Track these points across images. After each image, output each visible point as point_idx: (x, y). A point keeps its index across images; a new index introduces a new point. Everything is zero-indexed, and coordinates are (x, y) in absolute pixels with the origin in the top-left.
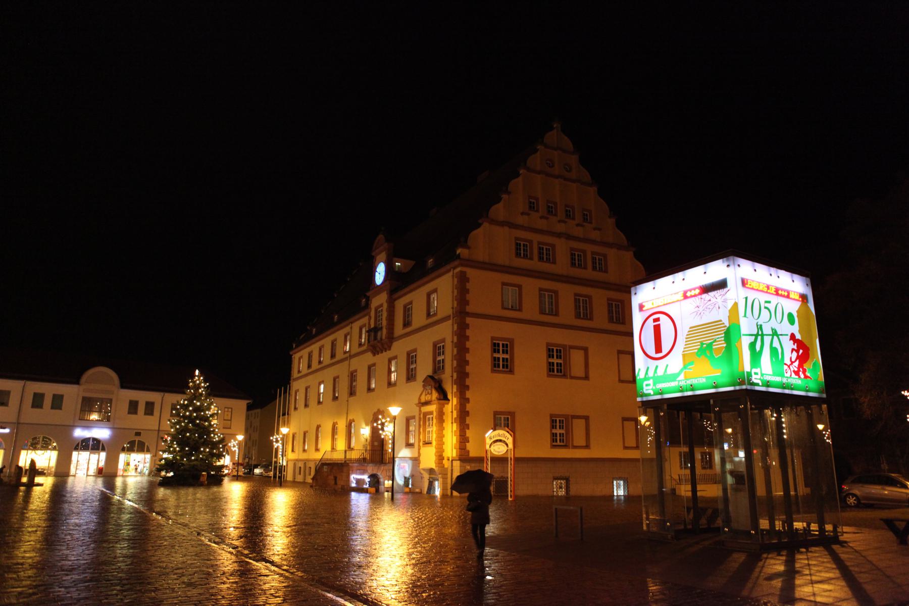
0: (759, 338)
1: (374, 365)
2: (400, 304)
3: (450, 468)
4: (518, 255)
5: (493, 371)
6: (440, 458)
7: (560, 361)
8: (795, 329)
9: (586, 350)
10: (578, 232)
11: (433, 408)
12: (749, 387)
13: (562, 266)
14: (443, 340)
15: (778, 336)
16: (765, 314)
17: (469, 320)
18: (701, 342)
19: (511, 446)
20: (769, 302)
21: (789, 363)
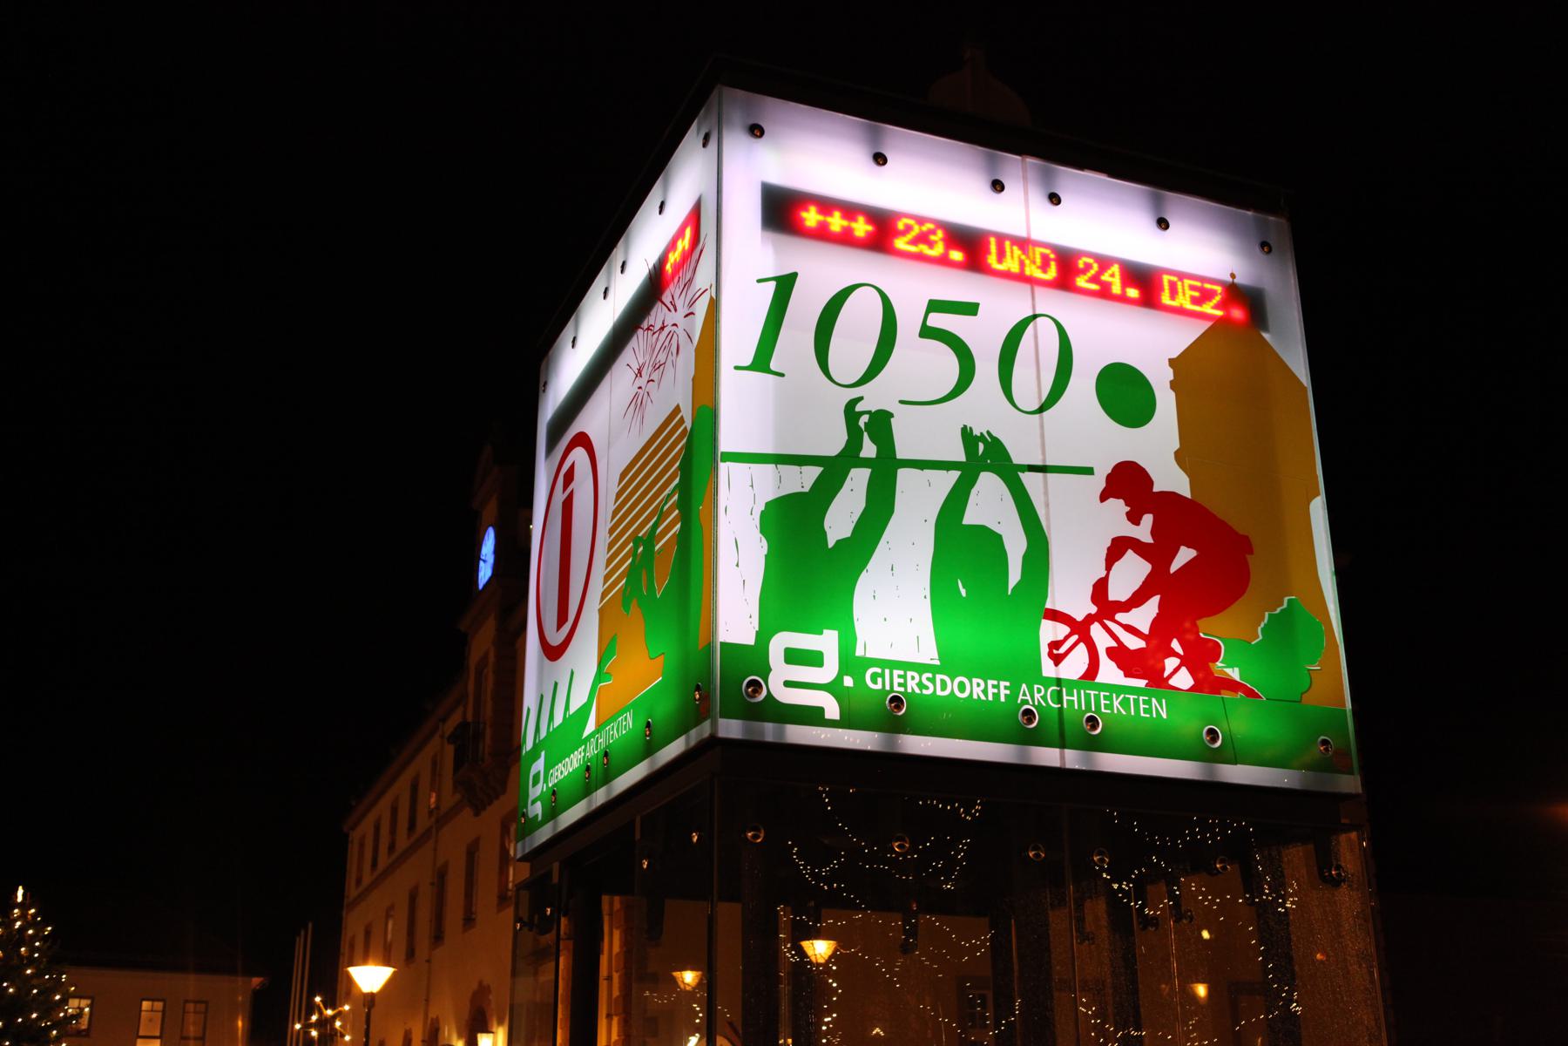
0: (858, 479)
8: (1157, 448)
12: (731, 728)
15: (1010, 473)
16: (921, 367)
20: (970, 309)
21: (1081, 607)
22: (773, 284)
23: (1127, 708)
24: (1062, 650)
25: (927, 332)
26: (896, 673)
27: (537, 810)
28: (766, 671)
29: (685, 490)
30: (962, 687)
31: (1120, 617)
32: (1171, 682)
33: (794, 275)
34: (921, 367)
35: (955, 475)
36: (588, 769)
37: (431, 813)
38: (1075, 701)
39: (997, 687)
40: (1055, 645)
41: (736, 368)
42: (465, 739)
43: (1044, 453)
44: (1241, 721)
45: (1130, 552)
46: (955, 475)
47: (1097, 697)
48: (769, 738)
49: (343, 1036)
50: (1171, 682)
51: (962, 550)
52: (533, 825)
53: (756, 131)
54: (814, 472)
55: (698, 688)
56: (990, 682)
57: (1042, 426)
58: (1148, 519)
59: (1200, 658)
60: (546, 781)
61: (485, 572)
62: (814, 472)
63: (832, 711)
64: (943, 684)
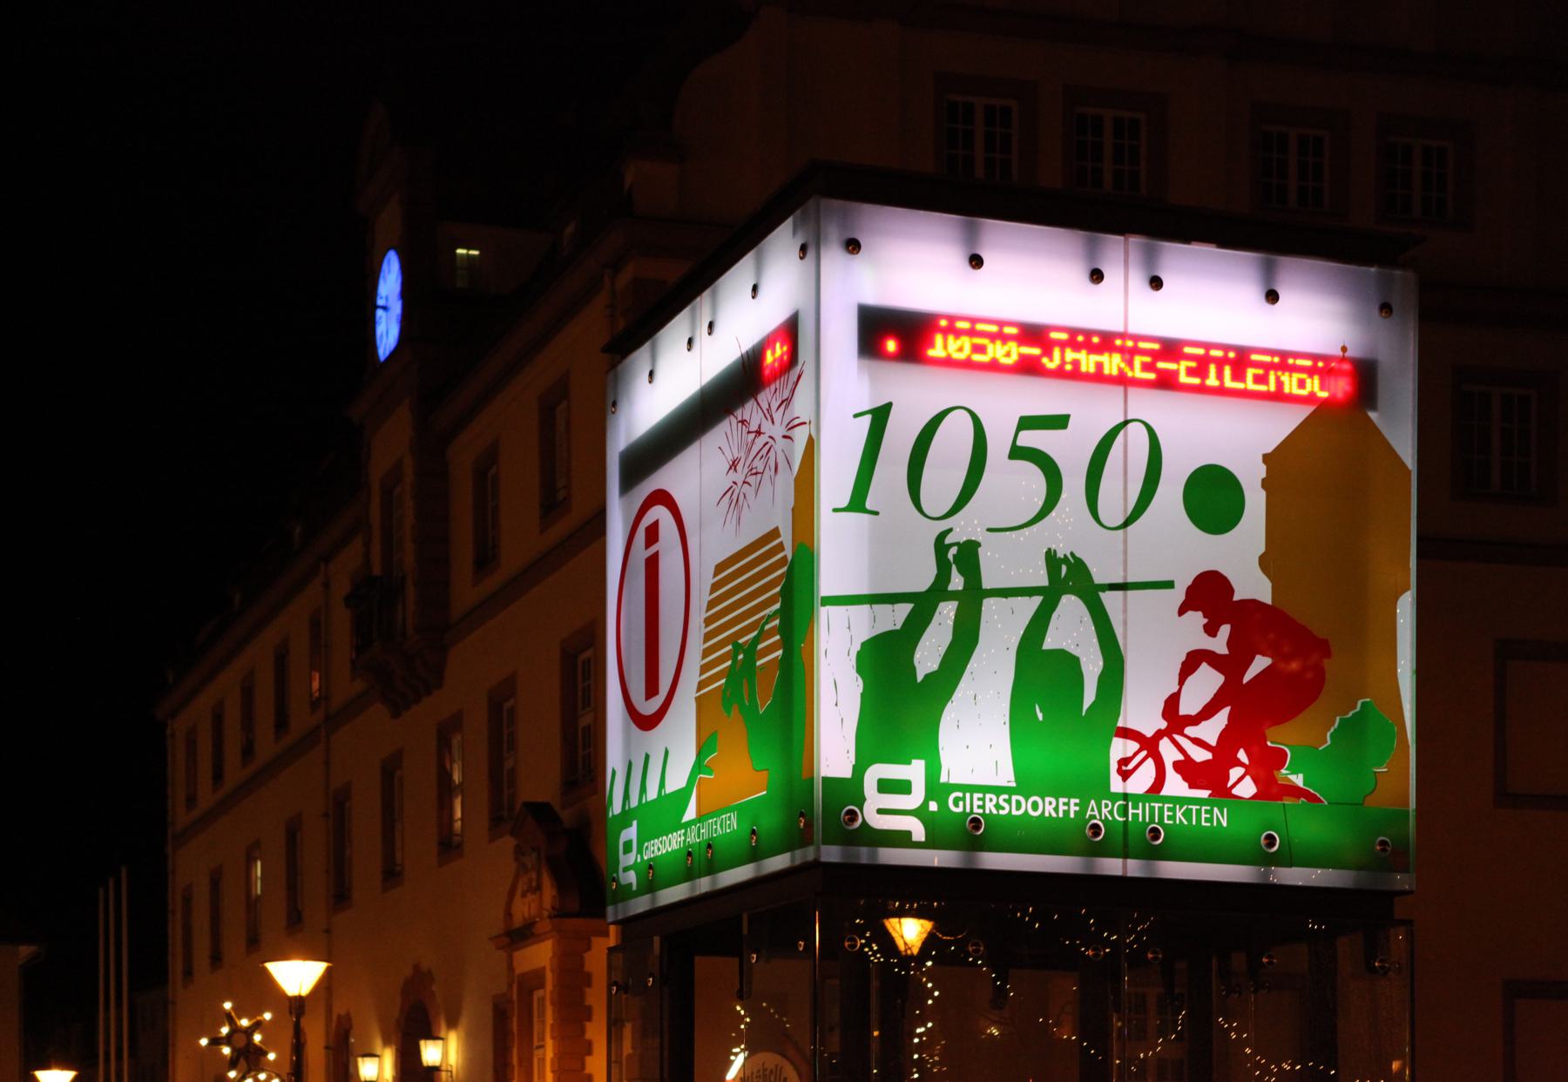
0: (947, 611)
8: (1241, 557)
11: (540, 955)
12: (832, 854)
15: (1091, 594)
16: (1011, 487)
18: (732, 639)
20: (1060, 422)
21: (1149, 721)
22: (868, 418)
23: (1189, 819)
24: (1130, 767)
25: (1017, 453)
26: (976, 796)
27: (631, 878)
28: (861, 800)
29: (786, 614)
30: (1035, 806)
31: (1189, 731)
32: (1234, 791)
33: (890, 405)
34: (1011, 487)
35: (1037, 600)
36: (689, 854)
37: (315, 704)
38: (1137, 812)
39: (1067, 804)
40: (1124, 761)
41: (835, 510)
42: (372, 600)
43: (1125, 570)
44: (1305, 826)
45: (1204, 665)
46: (1037, 600)
47: (1161, 809)
48: (864, 860)
49: (265, 1053)
50: (1234, 791)
51: (1043, 675)
52: (625, 893)
53: (853, 246)
54: (904, 609)
55: (802, 815)
56: (1062, 800)
57: (1125, 541)
58: (1225, 630)
59: (1266, 767)
60: (639, 851)
61: (387, 332)
62: (904, 609)
63: (918, 832)
64: (1018, 802)
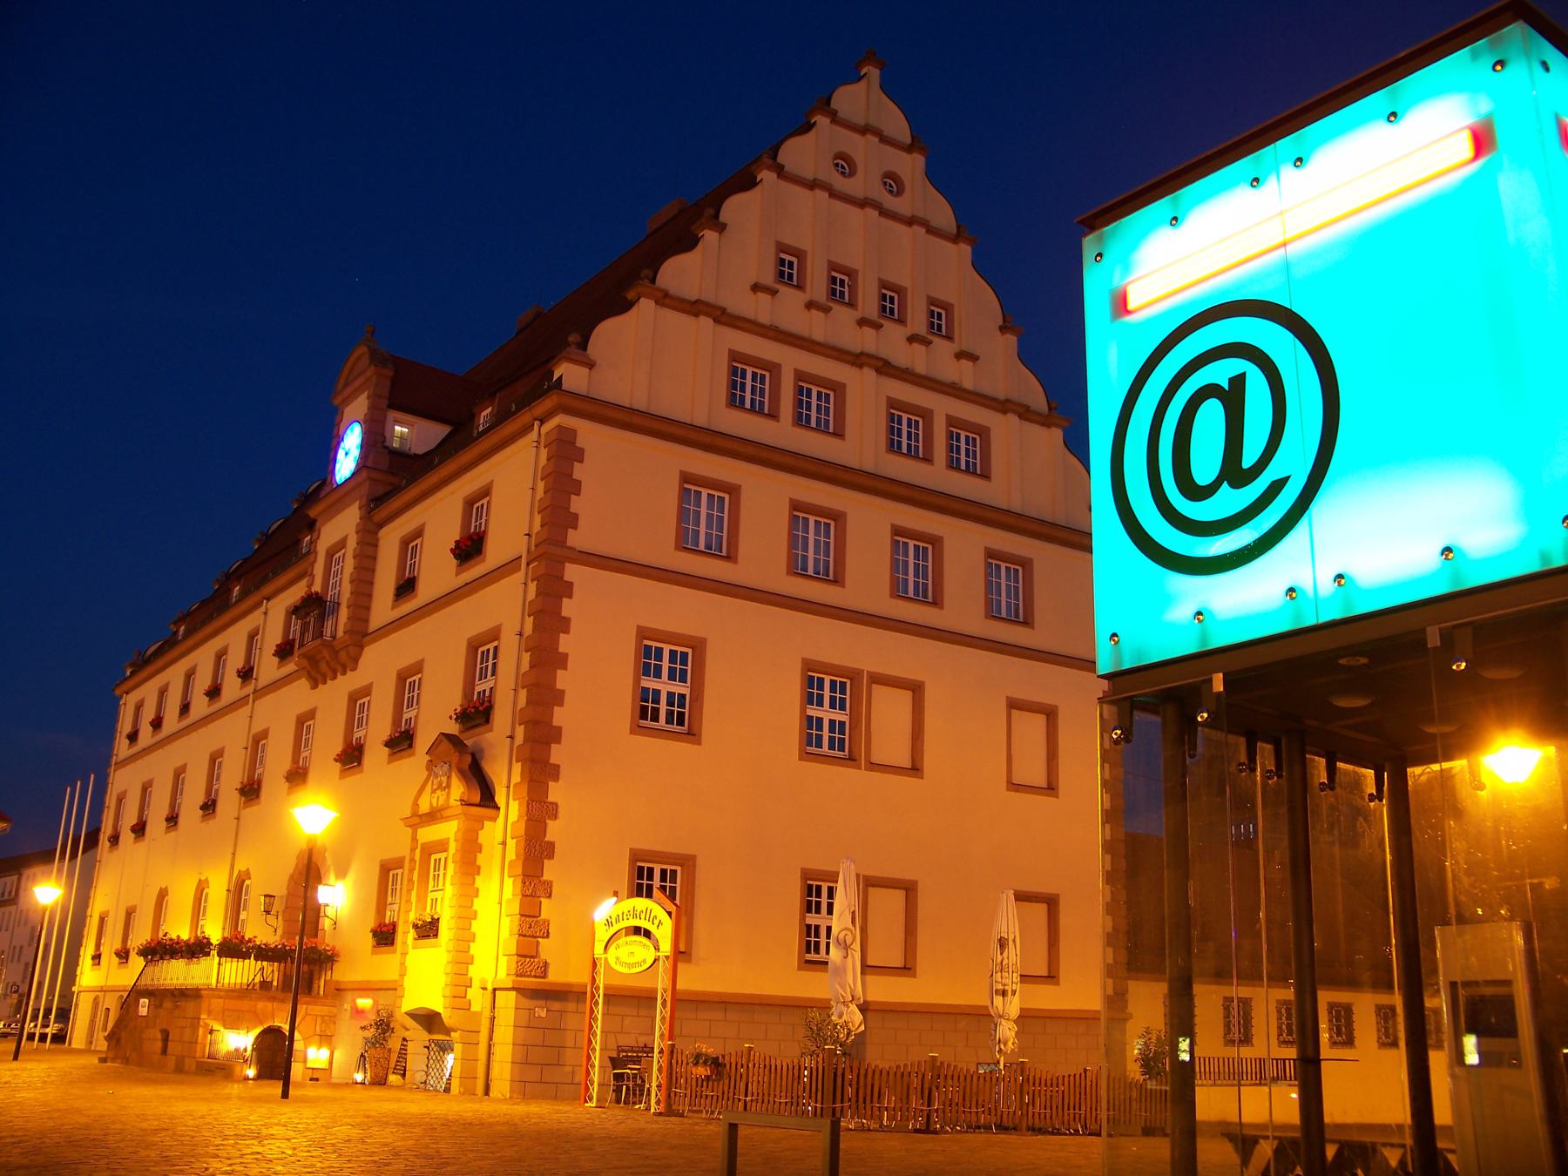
1: (311, 714)
2: (390, 539)
3: (487, 1013)
4: (735, 402)
5: (636, 729)
6: (460, 982)
7: (839, 716)
9: (916, 689)
10: (916, 358)
11: (448, 830)
13: (862, 443)
14: (494, 634)
17: (572, 572)
19: (666, 947)
